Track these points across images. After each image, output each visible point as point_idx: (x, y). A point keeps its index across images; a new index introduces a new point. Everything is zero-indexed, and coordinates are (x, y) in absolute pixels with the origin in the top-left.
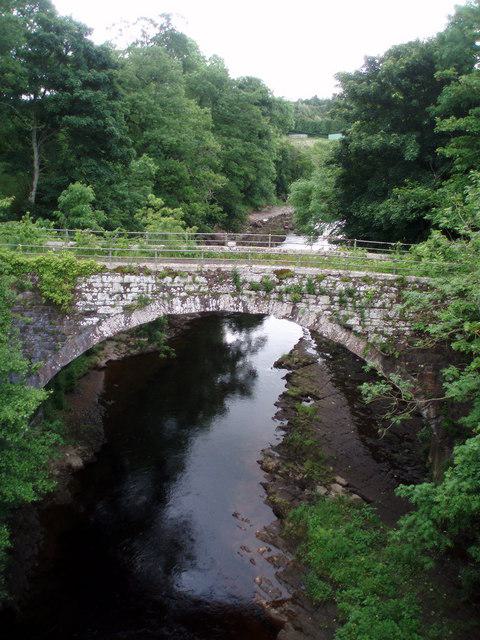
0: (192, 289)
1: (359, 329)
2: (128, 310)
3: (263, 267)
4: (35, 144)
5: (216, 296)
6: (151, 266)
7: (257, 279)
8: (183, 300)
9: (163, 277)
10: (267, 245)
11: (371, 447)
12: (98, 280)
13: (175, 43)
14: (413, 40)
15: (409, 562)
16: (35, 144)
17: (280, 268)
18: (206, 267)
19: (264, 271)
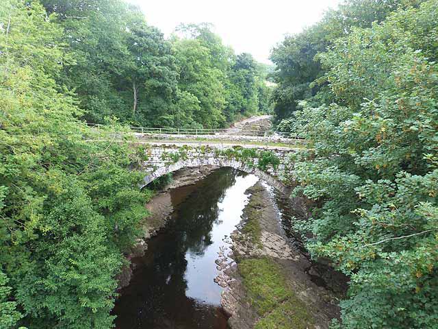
0: (196, 155)
1: (273, 174)
2: (168, 164)
3: (227, 145)
4: (134, 85)
5: (207, 158)
6: (177, 145)
7: (225, 150)
8: (192, 160)
9: (182, 149)
10: (195, 134)
11: (286, 230)
12: (154, 151)
13: (206, 37)
14: (281, 40)
15: (81, 233)
16: (134, 85)
17: (235, 145)
18: (202, 145)
19: (228, 146)
